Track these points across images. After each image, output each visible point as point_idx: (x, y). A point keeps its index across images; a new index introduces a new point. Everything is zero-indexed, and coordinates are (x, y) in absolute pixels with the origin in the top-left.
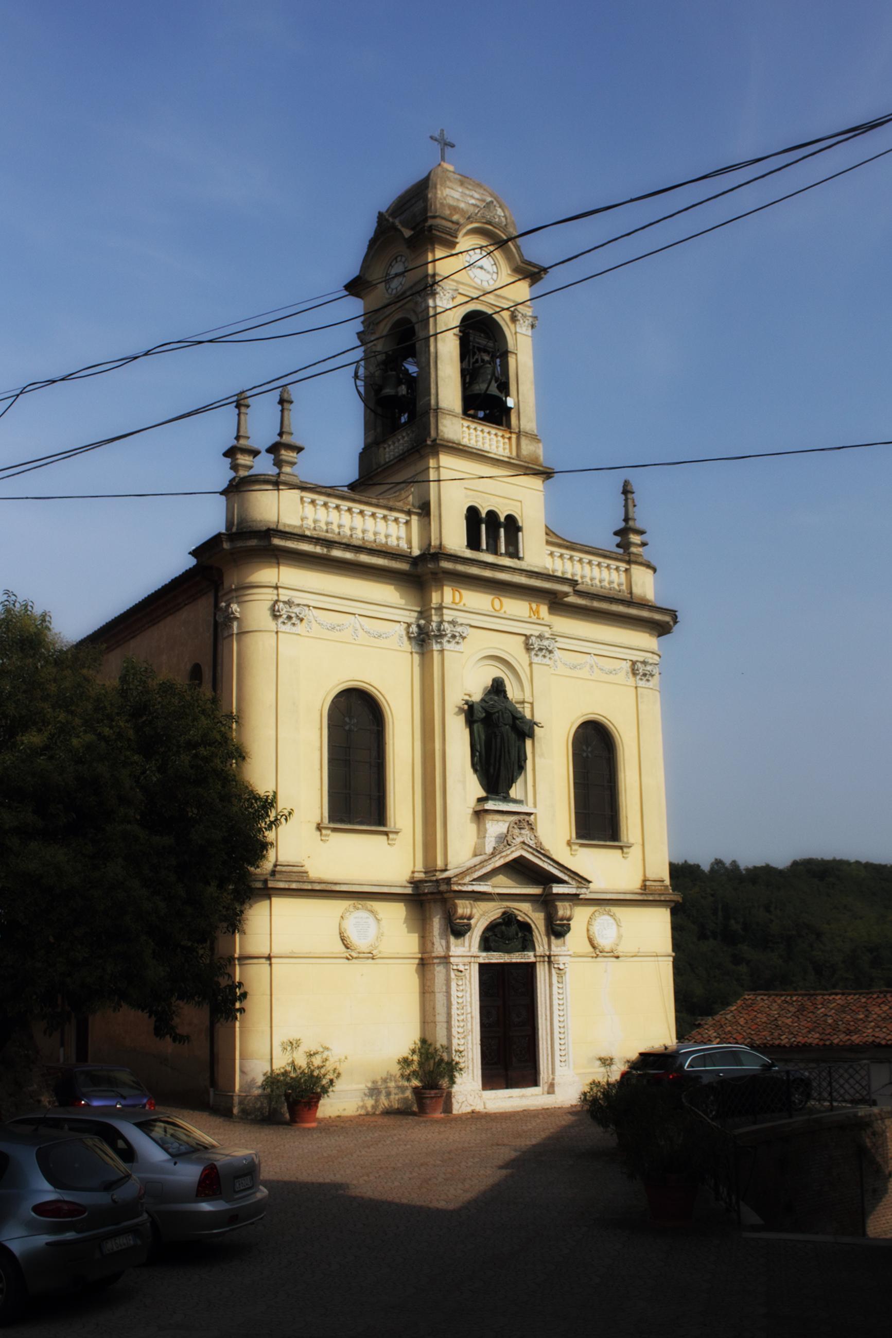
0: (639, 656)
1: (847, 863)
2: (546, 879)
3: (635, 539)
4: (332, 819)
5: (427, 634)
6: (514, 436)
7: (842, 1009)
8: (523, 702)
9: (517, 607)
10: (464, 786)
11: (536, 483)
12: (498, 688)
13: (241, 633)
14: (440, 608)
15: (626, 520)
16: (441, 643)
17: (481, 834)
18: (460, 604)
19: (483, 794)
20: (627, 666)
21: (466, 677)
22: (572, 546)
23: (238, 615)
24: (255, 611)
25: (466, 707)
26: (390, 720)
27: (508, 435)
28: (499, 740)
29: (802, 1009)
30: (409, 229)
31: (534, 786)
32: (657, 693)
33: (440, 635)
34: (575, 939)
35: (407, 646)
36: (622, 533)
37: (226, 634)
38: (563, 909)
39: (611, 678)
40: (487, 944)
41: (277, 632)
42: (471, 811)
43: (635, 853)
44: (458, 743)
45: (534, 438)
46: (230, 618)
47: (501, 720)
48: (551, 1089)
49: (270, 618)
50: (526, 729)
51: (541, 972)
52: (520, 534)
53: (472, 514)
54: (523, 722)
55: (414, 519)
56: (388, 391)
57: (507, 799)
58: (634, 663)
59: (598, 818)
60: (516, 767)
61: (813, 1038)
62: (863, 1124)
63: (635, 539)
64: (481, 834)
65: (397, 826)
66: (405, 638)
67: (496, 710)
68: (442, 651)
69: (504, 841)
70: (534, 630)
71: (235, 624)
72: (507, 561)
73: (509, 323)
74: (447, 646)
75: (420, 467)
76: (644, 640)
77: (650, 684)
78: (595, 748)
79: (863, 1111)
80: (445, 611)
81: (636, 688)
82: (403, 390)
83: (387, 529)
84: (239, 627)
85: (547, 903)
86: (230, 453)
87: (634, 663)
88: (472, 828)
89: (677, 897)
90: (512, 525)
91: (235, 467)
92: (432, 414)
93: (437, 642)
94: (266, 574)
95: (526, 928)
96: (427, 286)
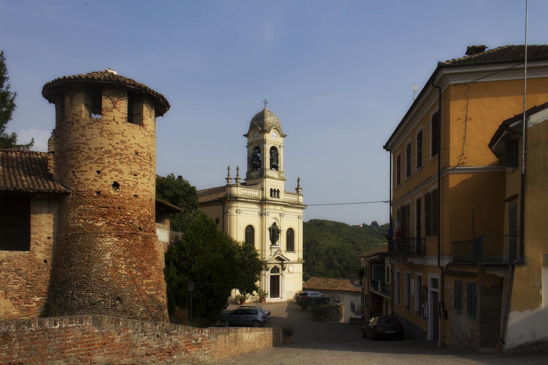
0: (299, 215)
1: (327, 221)
2: (283, 260)
3: (300, 190)
7: (333, 282)
9: (278, 208)
10: (268, 242)
11: (283, 182)
14: (265, 209)
15: (298, 186)
17: (271, 251)
18: (269, 208)
21: (269, 223)
22: (288, 193)
24: (233, 211)
29: (325, 281)
30: (258, 125)
34: (286, 271)
35: (258, 216)
36: (297, 189)
38: (285, 265)
40: (271, 272)
43: (297, 253)
45: (283, 173)
46: (227, 212)
48: (282, 298)
51: (280, 277)
53: (271, 189)
56: (254, 163)
57: (276, 245)
59: (290, 247)
61: (327, 288)
62: (338, 306)
63: (300, 190)
64: (271, 251)
69: (276, 253)
70: (281, 212)
72: (277, 199)
75: (261, 180)
76: (301, 211)
78: (291, 233)
79: (339, 304)
82: (258, 163)
83: (254, 193)
85: (282, 264)
86: (227, 179)
89: (304, 262)
91: (228, 182)
94: (235, 205)
95: (278, 269)
96: (264, 142)
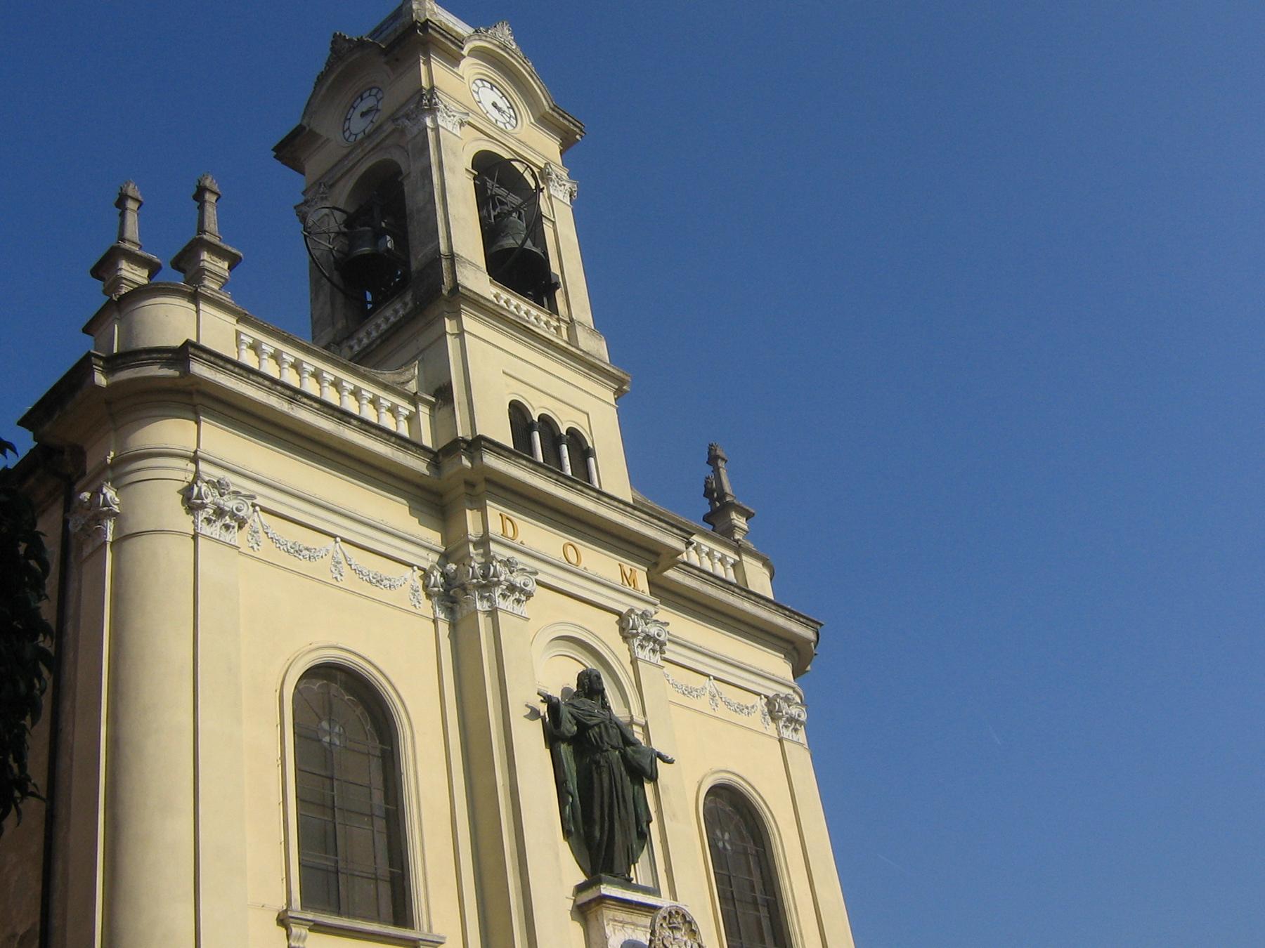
4: (307, 903)
5: (464, 588)
13: (122, 538)
16: (489, 599)
20: (761, 703)
23: (116, 509)
24: (156, 500)
25: (543, 708)
33: (487, 585)
35: (427, 607)
37: (87, 550)
39: (741, 718)
41: (195, 537)
42: (569, 904)
50: (646, 763)
52: (592, 460)
54: (639, 752)
55: (424, 411)
58: (770, 702)
65: (436, 930)
66: (422, 594)
67: (596, 721)
68: (493, 613)
71: (110, 525)
74: (501, 603)
84: (118, 528)
88: (576, 929)
92: (445, 264)
93: (482, 598)
94: (173, 432)
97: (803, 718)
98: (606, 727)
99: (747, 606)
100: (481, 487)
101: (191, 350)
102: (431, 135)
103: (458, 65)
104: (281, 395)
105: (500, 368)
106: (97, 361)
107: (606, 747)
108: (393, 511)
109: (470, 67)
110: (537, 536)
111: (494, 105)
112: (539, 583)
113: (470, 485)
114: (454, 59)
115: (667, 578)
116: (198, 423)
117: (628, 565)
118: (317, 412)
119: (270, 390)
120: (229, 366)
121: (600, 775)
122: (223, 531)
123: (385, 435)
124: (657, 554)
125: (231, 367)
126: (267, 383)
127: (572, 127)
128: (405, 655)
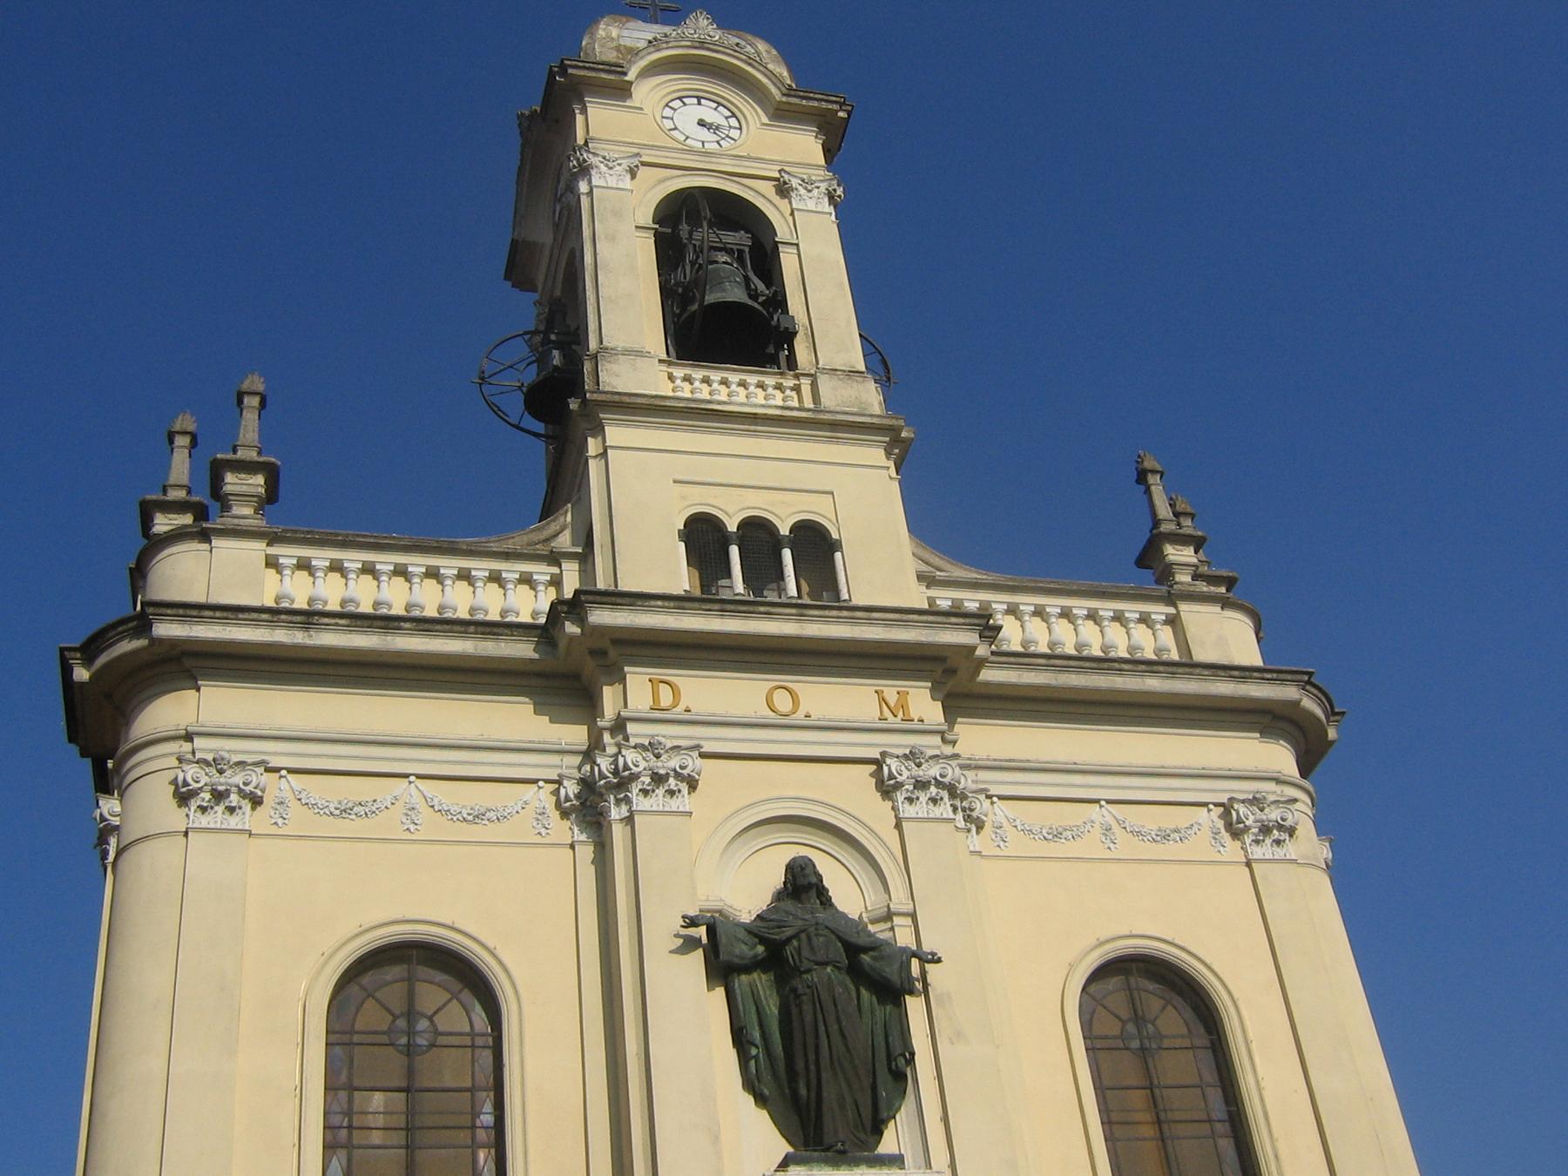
6: (805, 384)
8: (889, 916)
12: (802, 884)
16: (628, 801)
19: (785, 1148)
20: (1210, 819)
23: (116, 821)
26: (514, 1007)
27: (790, 383)
28: (807, 1008)
31: (945, 1119)
32: (874, 454)
39: (1170, 850)
44: (692, 1027)
47: (806, 952)
49: (173, 803)
50: (891, 972)
52: (838, 555)
58: (1226, 808)
60: (883, 1076)
67: (789, 932)
68: (629, 820)
73: (776, 199)
74: (640, 803)
77: (1291, 849)
80: (631, 728)
81: (1248, 864)
87: (1226, 808)
90: (815, 545)
93: (618, 802)
97: (870, 927)
98: (809, 939)
99: (1154, 684)
100: (613, 653)
101: (150, 610)
102: (585, 201)
103: (630, 96)
104: (291, 625)
105: (664, 475)
106: (72, 654)
107: (806, 965)
108: (514, 719)
109: (649, 93)
110: (707, 691)
111: (701, 123)
112: (703, 756)
113: (598, 653)
114: (621, 91)
115: (987, 684)
116: (198, 690)
117: (891, 689)
118: (349, 629)
119: (272, 624)
120: (207, 613)
121: (799, 1006)
122: (227, 816)
123: (458, 628)
124: (943, 659)
125: (210, 613)
126: (264, 616)
127: (824, 105)
128: (512, 898)
